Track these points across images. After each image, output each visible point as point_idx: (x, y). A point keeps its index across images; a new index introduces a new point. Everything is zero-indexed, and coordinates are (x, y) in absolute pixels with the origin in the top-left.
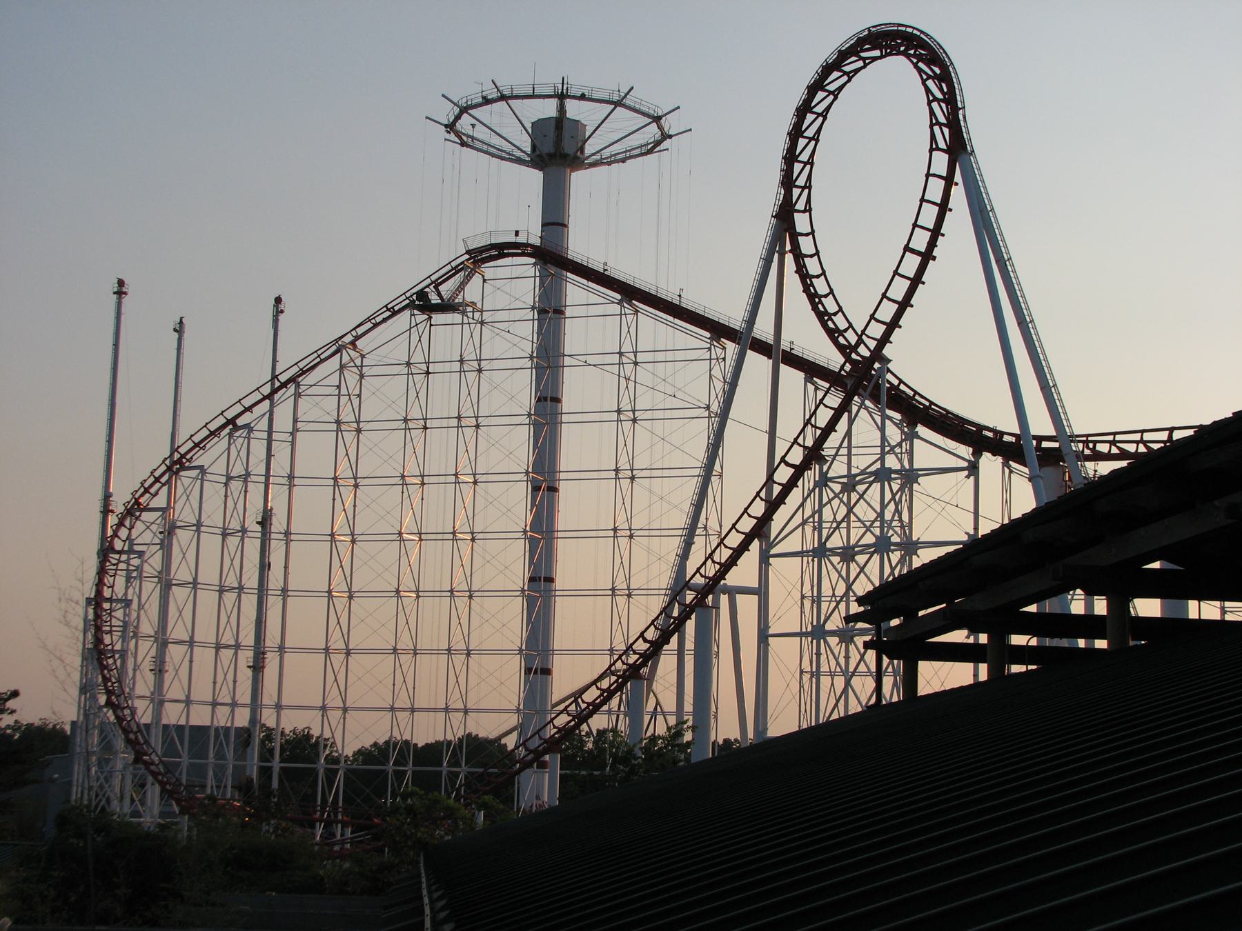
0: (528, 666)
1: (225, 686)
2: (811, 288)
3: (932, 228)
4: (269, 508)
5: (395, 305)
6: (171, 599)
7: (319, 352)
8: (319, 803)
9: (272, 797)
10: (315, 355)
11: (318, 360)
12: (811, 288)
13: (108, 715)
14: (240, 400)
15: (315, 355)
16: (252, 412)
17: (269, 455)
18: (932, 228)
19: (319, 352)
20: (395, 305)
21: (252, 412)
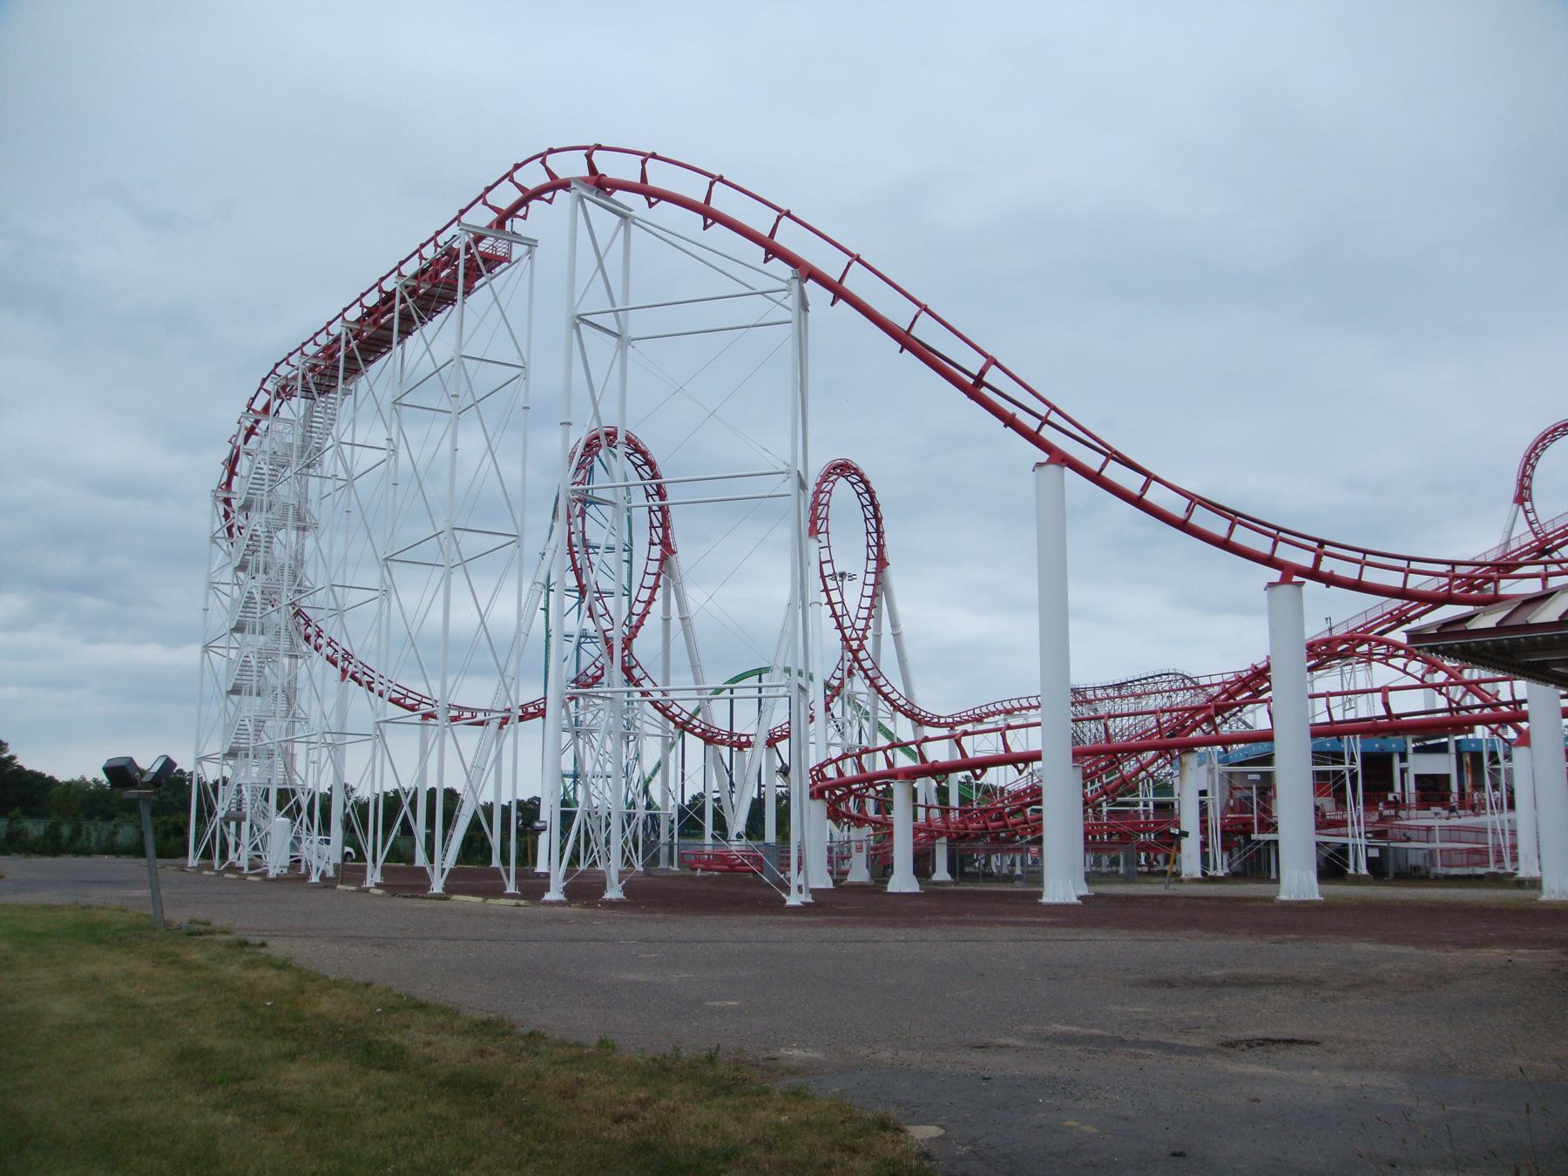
0: (1494, 784)
1: (1348, 679)
2: (1394, 613)
3: (1362, 579)
4: (1080, 902)
5: (368, 675)
6: (424, 844)
7: (1054, 417)
8: (1428, 743)
9: (1414, 737)
10: (1042, 409)
11: (1033, 424)
12: (1394, 613)
13: (638, 1130)
14: (788, 214)
15: (1042, 409)
16: (706, 227)
17: (221, 602)
18: (1362, 579)
19: (1054, 417)
20: (368, 675)
21: (706, 227)
